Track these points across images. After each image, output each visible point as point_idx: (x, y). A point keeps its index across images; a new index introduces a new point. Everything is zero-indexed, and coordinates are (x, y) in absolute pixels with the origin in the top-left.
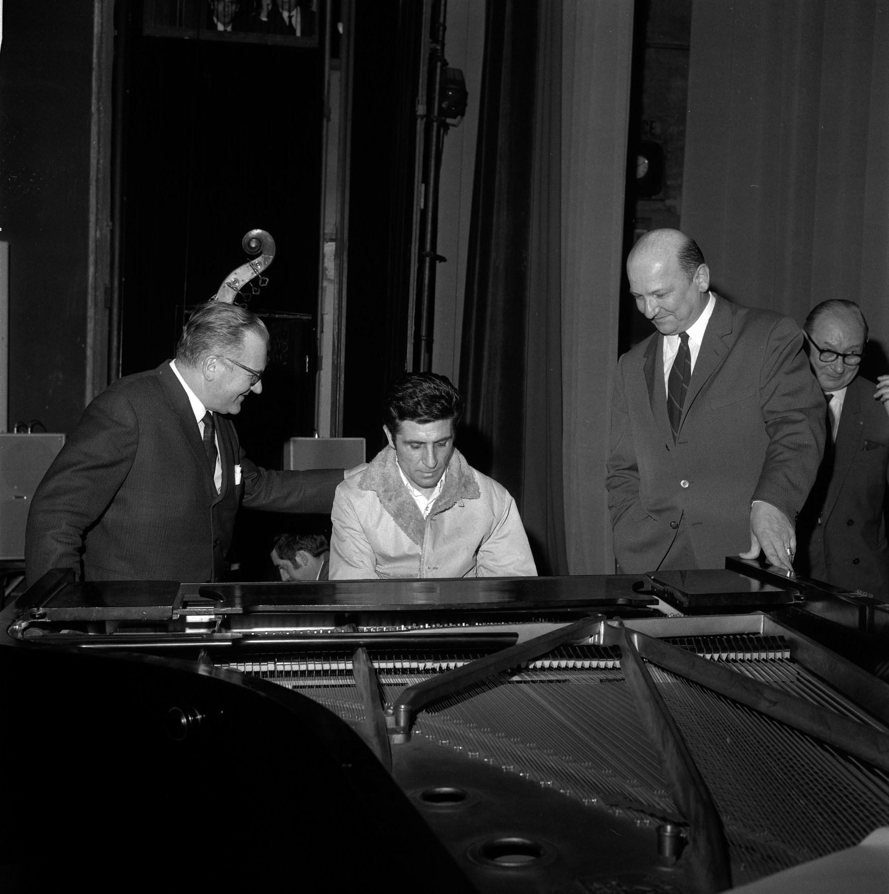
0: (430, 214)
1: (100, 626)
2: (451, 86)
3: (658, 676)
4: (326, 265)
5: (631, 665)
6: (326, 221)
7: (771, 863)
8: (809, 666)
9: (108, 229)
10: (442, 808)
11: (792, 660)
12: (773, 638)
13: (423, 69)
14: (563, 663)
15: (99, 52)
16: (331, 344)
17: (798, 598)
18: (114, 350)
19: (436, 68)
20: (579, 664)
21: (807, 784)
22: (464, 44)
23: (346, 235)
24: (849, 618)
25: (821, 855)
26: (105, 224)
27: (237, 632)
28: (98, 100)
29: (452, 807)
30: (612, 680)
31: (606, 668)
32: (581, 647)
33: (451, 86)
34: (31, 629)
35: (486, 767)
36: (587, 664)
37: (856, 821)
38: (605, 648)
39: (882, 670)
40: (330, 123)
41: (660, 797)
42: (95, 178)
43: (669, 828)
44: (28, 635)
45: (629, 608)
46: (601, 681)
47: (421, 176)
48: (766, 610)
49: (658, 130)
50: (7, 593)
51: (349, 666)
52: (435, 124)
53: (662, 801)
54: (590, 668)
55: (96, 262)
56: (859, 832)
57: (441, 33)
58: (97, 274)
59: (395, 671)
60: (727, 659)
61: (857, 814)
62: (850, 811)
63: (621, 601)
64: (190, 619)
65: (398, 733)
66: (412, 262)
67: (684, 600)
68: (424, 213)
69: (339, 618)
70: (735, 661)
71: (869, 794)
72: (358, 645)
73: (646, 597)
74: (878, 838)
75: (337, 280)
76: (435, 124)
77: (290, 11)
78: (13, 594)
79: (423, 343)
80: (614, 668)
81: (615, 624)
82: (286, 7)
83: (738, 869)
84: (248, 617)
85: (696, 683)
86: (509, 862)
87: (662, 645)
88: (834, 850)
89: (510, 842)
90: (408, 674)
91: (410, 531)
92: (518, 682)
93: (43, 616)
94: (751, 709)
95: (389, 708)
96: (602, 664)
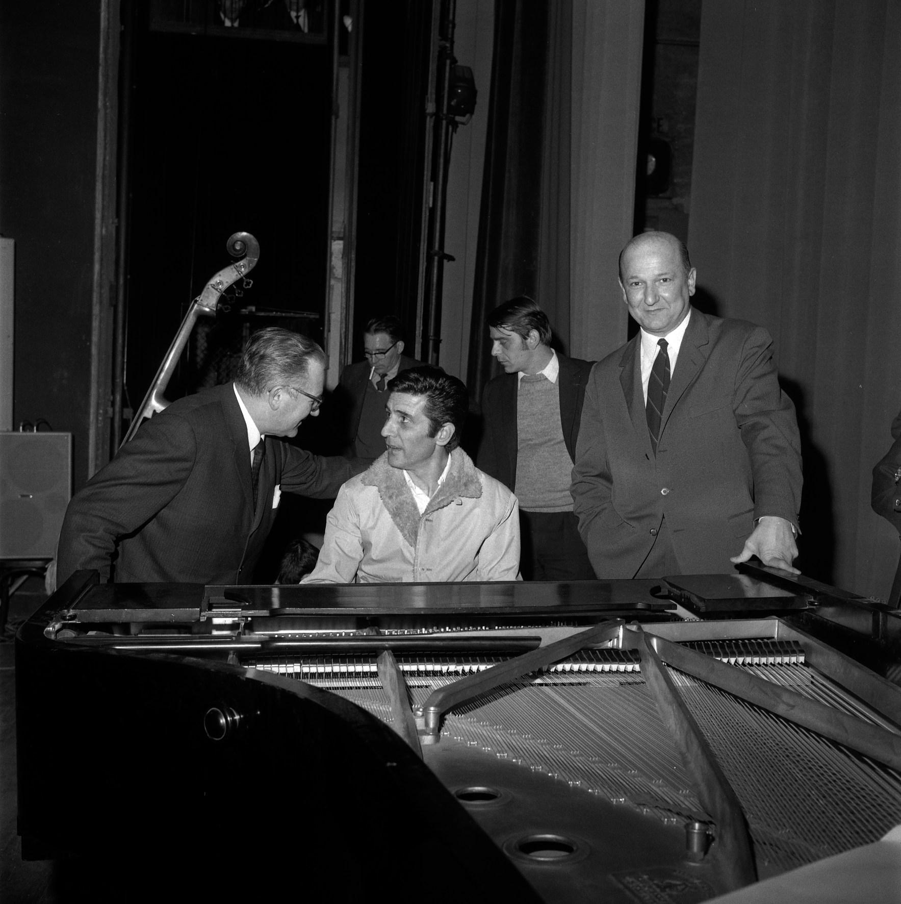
0: (439, 213)
1: (125, 627)
2: (461, 84)
3: (678, 680)
4: (333, 263)
5: (652, 669)
6: (334, 219)
7: (792, 859)
8: (823, 670)
9: (114, 226)
10: (476, 806)
11: (806, 664)
12: (788, 642)
13: (433, 67)
14: (584, 667)
15: (106, 48)
16: (338, 344)
17: (812, 604)
18: (119, 348)
19: (445, 65)
20: (599, 667)
21: (826, 784)
22: (473, 42)
23: (354, 233)
24: (861, 623)
25: (841, 852)
26: (111, 221)
27: (260, 634)
28: (105, 95)
29: (484, 805)
30: (631, 684)
31: (625, 672)
32: (602, 651)
33: (461, 84)
34: (64, 631)
35: (515, 766)
36: (607, 667)
37: (874, 821)
38: (624, 652)
39: (894, 675)
40: (338, 120)
41: (685, 796)
42: (101, 174)
43: (697, 825)
44: (60, 637)
45: (648, 613)
46: (621, 684)
47: (430, 174)
48: (780, 614)
49: (665, 127)
50: (10, 592)
51: (374, 668)
52: (444, 122)
53: (685, 799)
54: (610, 671)
55: (102, 260)
56: (877, 830)
57: (450, 30)
58: (101, 271)
59: (419, 673)
60: (743, 664)
61: (874, 814)
62: (868, 811)
63: (640, 606)
64: (216, 621)
65: (429, 734)
66: (421, 262)
67: (701, 604)
68: (432, 211)
69: (361, 621)
70: (751, 665)
71: (886, 795)
72: (385, 649)
73: (661, 602)
74: (894, 836)
75: (344, 279)
76: (444, 122)
77: (298, 11)
78: (18, 593)
79: (431, 343)
80: (633, 671)
81: (634, 628)
82: (295, 7)
83: (763, 864)
84: (276, 618)
85: (715, 687)
86: (544, 857)
87: (681, 650)
88: (853, 847)
89: (546, 839)
90: (435, 678)
91: (406, 532)
92: (541, 685)
93: (73, 617)
94: (768, 712)
95: (418, 710)
96: (622, 667)
